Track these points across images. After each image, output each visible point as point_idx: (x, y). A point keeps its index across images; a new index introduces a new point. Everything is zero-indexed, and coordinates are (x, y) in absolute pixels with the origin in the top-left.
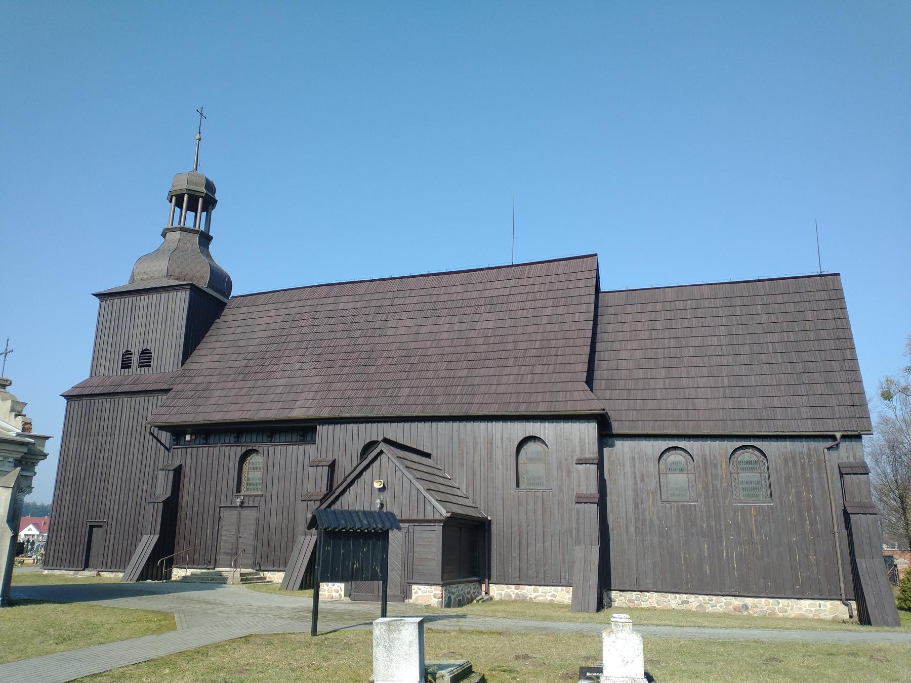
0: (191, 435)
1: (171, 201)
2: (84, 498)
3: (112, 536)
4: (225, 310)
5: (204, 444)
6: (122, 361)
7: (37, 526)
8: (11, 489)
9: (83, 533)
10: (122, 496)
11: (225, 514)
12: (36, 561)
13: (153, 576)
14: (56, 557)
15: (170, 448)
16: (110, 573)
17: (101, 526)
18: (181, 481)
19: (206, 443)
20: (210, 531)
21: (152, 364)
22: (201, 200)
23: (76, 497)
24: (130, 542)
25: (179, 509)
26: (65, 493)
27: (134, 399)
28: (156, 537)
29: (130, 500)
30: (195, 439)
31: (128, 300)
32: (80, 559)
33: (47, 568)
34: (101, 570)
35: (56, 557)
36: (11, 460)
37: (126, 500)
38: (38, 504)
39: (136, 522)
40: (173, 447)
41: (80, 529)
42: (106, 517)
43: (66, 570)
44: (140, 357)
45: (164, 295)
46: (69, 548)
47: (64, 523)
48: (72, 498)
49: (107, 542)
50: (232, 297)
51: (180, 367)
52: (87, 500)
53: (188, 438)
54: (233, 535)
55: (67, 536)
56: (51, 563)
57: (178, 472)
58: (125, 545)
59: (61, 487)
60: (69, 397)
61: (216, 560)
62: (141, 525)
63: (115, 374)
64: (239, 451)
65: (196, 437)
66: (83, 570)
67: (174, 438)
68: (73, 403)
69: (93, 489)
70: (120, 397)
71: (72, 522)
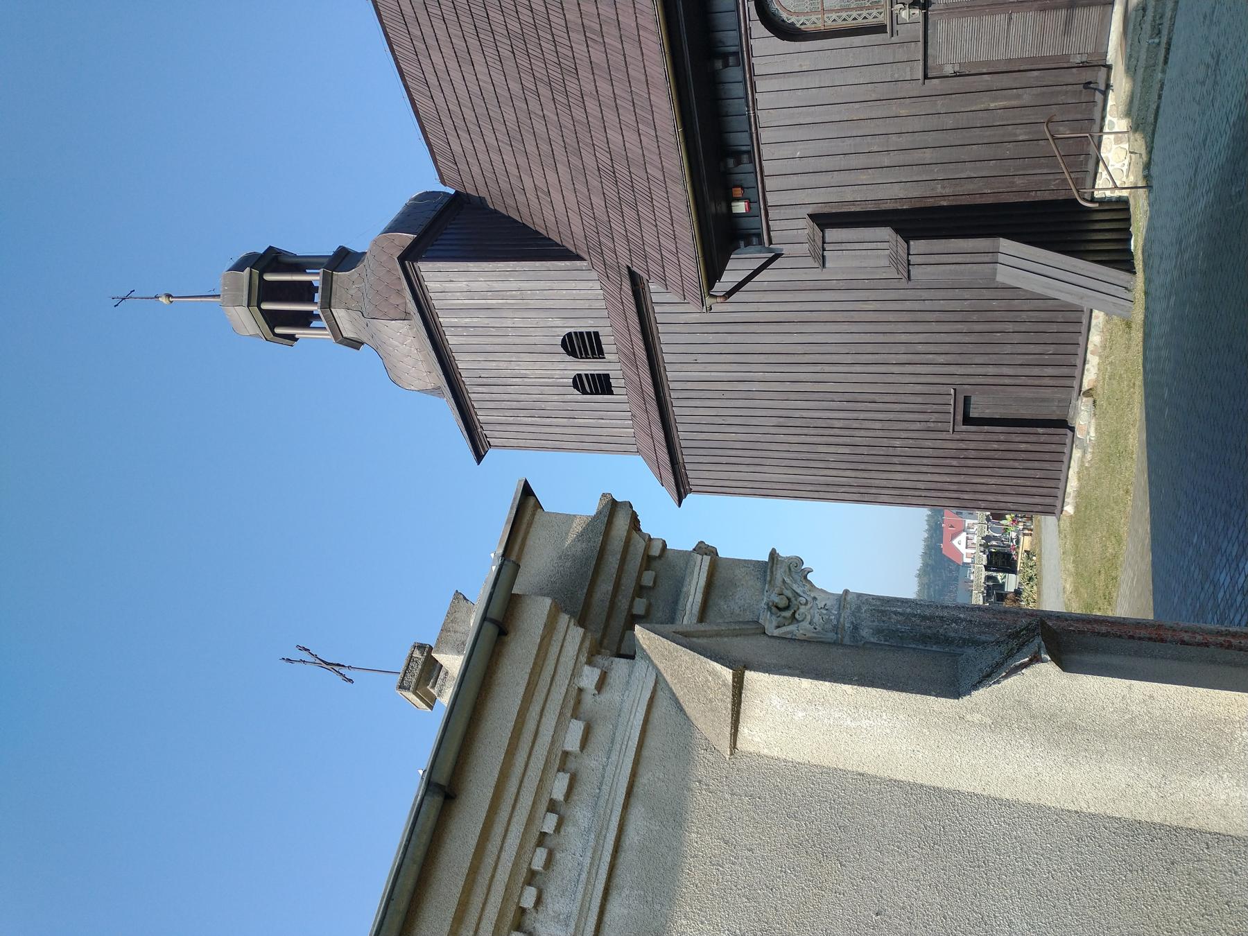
0: (730, 199)
1: (292, 338)
2: (897, 443)
3: (991, 370)
4: (469, 192)
5: (752, 161)
6: (597, 393)
7: (955, 535)
8: (749, 675)
9: (981, 437)
10: (893, 358)
11: (946, 58)
12: (1026, 532)
13: (1122, 237)
14: (1034, 490)
15: (770, 251)
16: (1087, 366)
17: (967, 400)
18: (853, 209)
19: (750, 153)
20: (995, 99)
21: (592, 330)
22: (269, 277)
23: (896, 460)
24: (1010, 327)
25: (930, 203)
26: (884, 483)
27: (667, 358)
28: (1005, 244)
29: (904, 338)
30: (743, 188)
31: (475, 395)
32: (1043, 439)
33: (1059, 507)
34: (1077, 388)
35: (1034, 490)
36: (589, 677)
37: (902, 348)
38: (926, 535)
39: (959, 317)
40: (767, 245)
41: (972, 445)
42: (943, 389)
43: (1069, 467)
44: (582, 358)
45: (444, 320)
46: (1016, 464)
47: (955, 479)
48: (899, 468)
49: (1007, 381)
50: (443, 182)
51: (585, 263)
52: (903, 435)
53: (740, 207)
54: (1010, 19)
55: (986, 471)
56: (1048, 501)
57: (824, 220)
58: (1017, 338)
59: (873, 491)
60: (681, 490)
61: (1084, 66)
62: (966, 303)
63: (626, 407)
64: (762, 42)
65: (737, 186)
66: (1072, 429)
67: (742, 244)
68: (692, 482)
69: (878, 425)
70: (666, 389)
71: (954, 462)
